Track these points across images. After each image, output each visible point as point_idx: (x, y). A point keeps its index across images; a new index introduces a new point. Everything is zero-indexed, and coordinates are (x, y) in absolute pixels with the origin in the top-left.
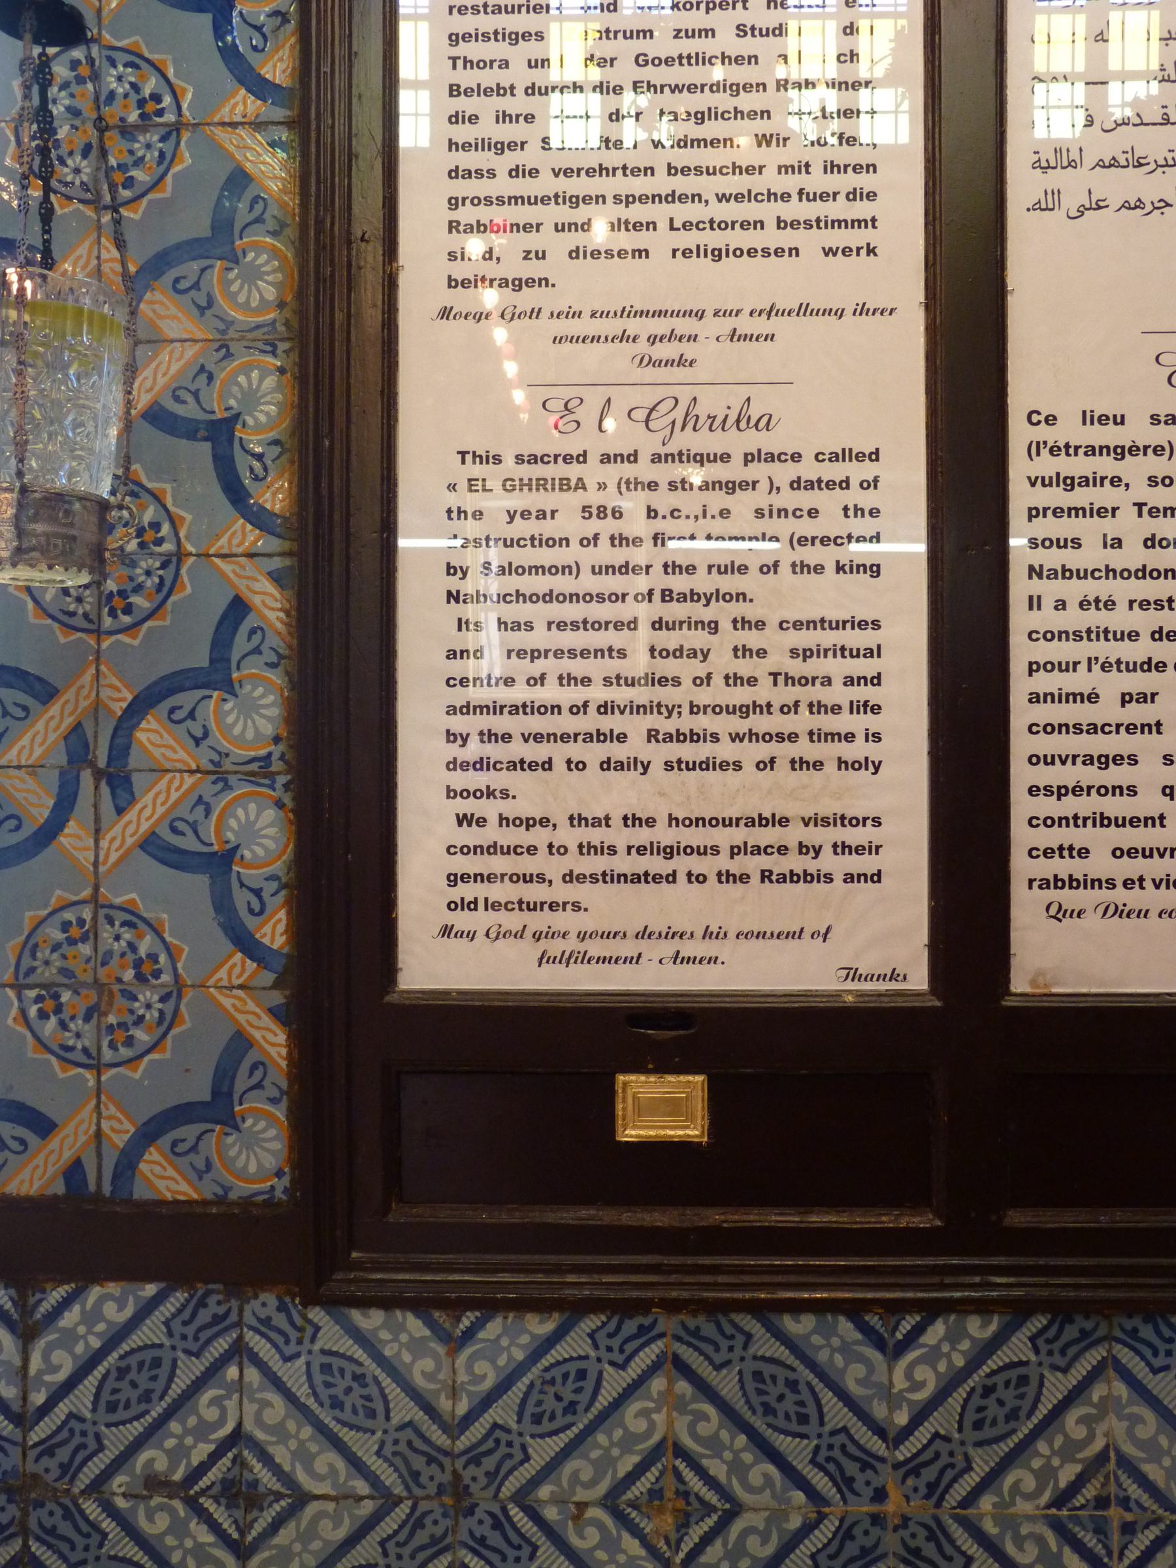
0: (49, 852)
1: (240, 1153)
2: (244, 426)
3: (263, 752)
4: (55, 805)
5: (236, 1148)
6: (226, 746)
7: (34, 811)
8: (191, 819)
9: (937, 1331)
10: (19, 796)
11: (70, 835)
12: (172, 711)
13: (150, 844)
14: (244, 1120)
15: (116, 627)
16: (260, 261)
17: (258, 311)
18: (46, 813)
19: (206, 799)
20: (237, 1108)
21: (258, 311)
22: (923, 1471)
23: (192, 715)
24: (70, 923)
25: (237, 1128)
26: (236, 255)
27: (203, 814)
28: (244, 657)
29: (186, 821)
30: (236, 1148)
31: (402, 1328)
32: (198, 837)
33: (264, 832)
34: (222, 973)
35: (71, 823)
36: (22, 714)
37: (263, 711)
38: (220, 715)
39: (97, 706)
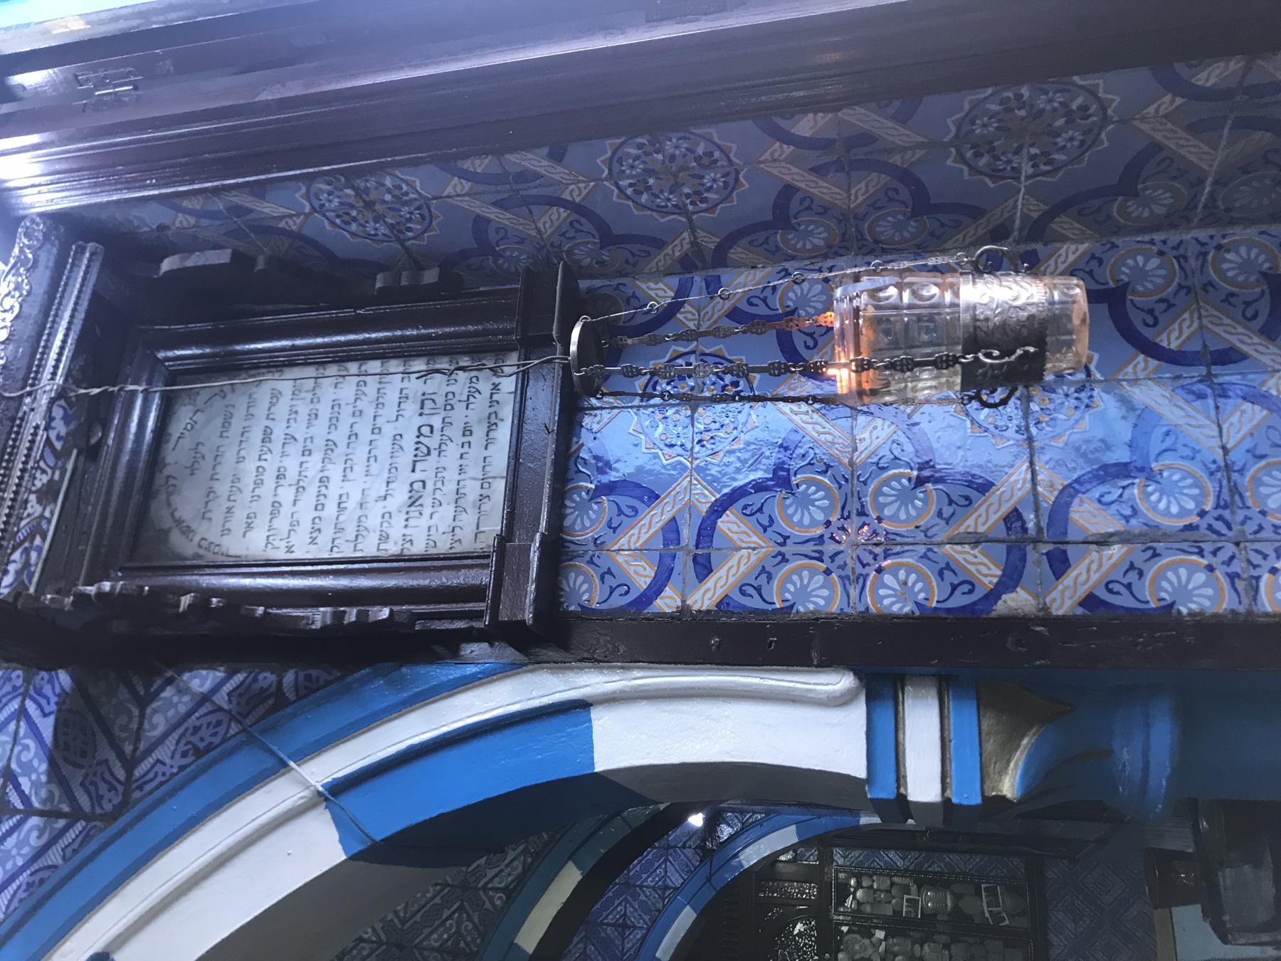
5: (916, 589)
6: (788, 530)
16: (792, 589)
17: (833, 591)
20: (780, 311)
21: (833, 591)
22: (101, 793)
28: (764, 600)
30: (916, 589)
31: (900, 597)
32: (761, 596)
34: (1152, 109)
37: (891, 592)
38: (927, 588)
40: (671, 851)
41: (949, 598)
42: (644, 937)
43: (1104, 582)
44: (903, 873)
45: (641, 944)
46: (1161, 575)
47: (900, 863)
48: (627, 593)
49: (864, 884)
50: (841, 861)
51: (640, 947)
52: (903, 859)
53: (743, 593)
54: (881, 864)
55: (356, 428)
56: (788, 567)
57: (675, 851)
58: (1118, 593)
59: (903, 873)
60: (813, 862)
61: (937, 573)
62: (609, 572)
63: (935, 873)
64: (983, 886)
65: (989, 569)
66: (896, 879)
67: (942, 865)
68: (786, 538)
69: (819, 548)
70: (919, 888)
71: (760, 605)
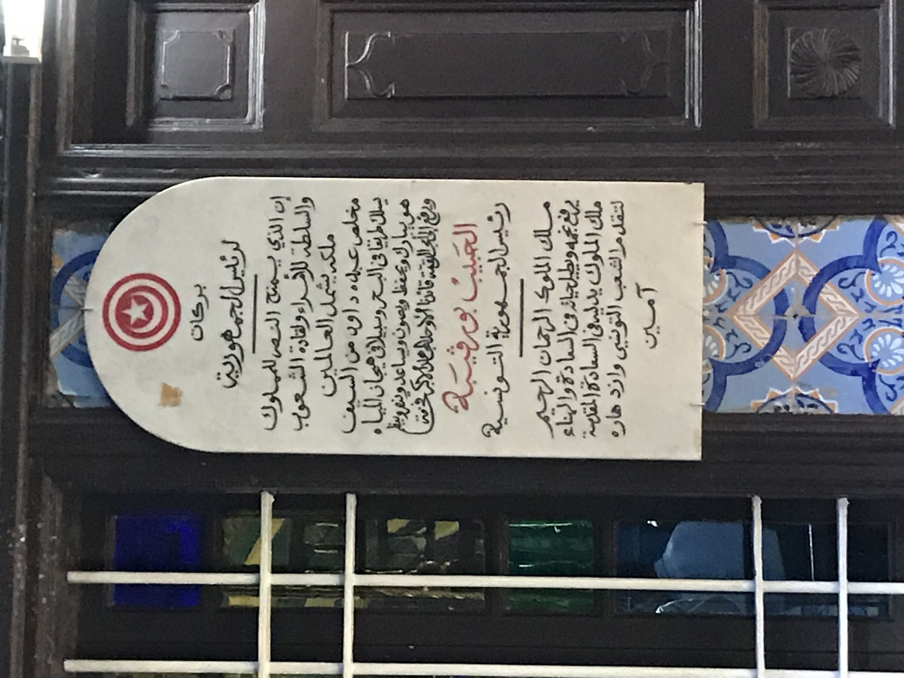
1: (881, 286)
2: (718, 356)
6: (874, 301)
11: (810, 275)
12: (841, 280)
13: (827, 360)
14: (883, 266)
23: (853, 283)
25: (880, 272)
27: (858, 341)
29: (848, 346)
33: (896, 351)
35: (808, 282)
38: (719, 347)
41: (734, 353)
43: (837, 344)
46: (874, 340)
48: (749, 350)
53: (840, 350)
55: (409, 217)
56: (874, 331)
58: (845, 352)
62: (733, 333)
65: (763, 333)
68: (873, 307)
69: (898, 316)
71: (856, 361)
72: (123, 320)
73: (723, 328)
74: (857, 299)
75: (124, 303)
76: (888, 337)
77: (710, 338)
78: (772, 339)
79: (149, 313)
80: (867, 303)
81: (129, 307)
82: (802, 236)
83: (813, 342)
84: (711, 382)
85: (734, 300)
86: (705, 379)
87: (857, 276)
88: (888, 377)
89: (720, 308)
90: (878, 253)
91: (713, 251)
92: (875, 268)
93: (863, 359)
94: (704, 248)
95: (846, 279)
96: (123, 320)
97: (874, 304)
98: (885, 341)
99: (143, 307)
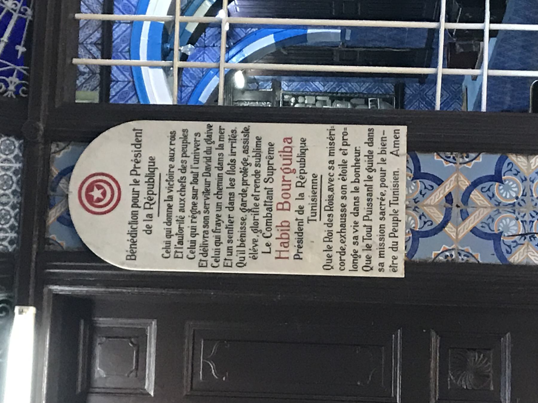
0: (440, 234)
3: (521, 223)
4: (444, 217)
7: (437, 220)
8: (487, 222)
9: (393, 87)
10: (432, 215)
14: (505, 181)
15: (464, 162)
18: (441, 220)
19: (492, 216)
24: (448, 256)
26: (502, 181)
28: (490, 229)
29: (486, 223)
36: (431, 188)
38: (415, 223)
39: (458, 187)
40: (206, 48)
42: (193, 91)
44: (324, 94)
45: (191, 94)
47: (322, 89)
49: (299, 101)
50: (286, 89)
51: (190, 96)
52: (324, 86)
54: (310, 89)
57: (209, 48)
59: (324, 94)
60: (269, 89)
61: (475, 226)
63: (342, 93)
64: (370, 99)
66: (319, 98)
67: (347, 88)
70: (332, 102)
72: (90, 198)
73: (417, 212)
74: (423, 215)
75: (90, 189)
76: (508, 220)
77: (410, 218)
78: (470, 193)
79: (104, 194)
80: (495, 200)
81: (92, 190)
82: (453, 249)
83: (467, 221)
84: (410, 242)
85: (490, 216)
86: (407, 240)
87: (423, 227)
88: (506, 241)
89: (416, 201)
90: (503, 174)
91: (413, 169)
92: (501, 181)
93: (420, 181)
94: (407, 167)
95: (485, 187)
96: (90, 198)
97: (500, 201)
98: (506, 222)
99: (101, 191)
